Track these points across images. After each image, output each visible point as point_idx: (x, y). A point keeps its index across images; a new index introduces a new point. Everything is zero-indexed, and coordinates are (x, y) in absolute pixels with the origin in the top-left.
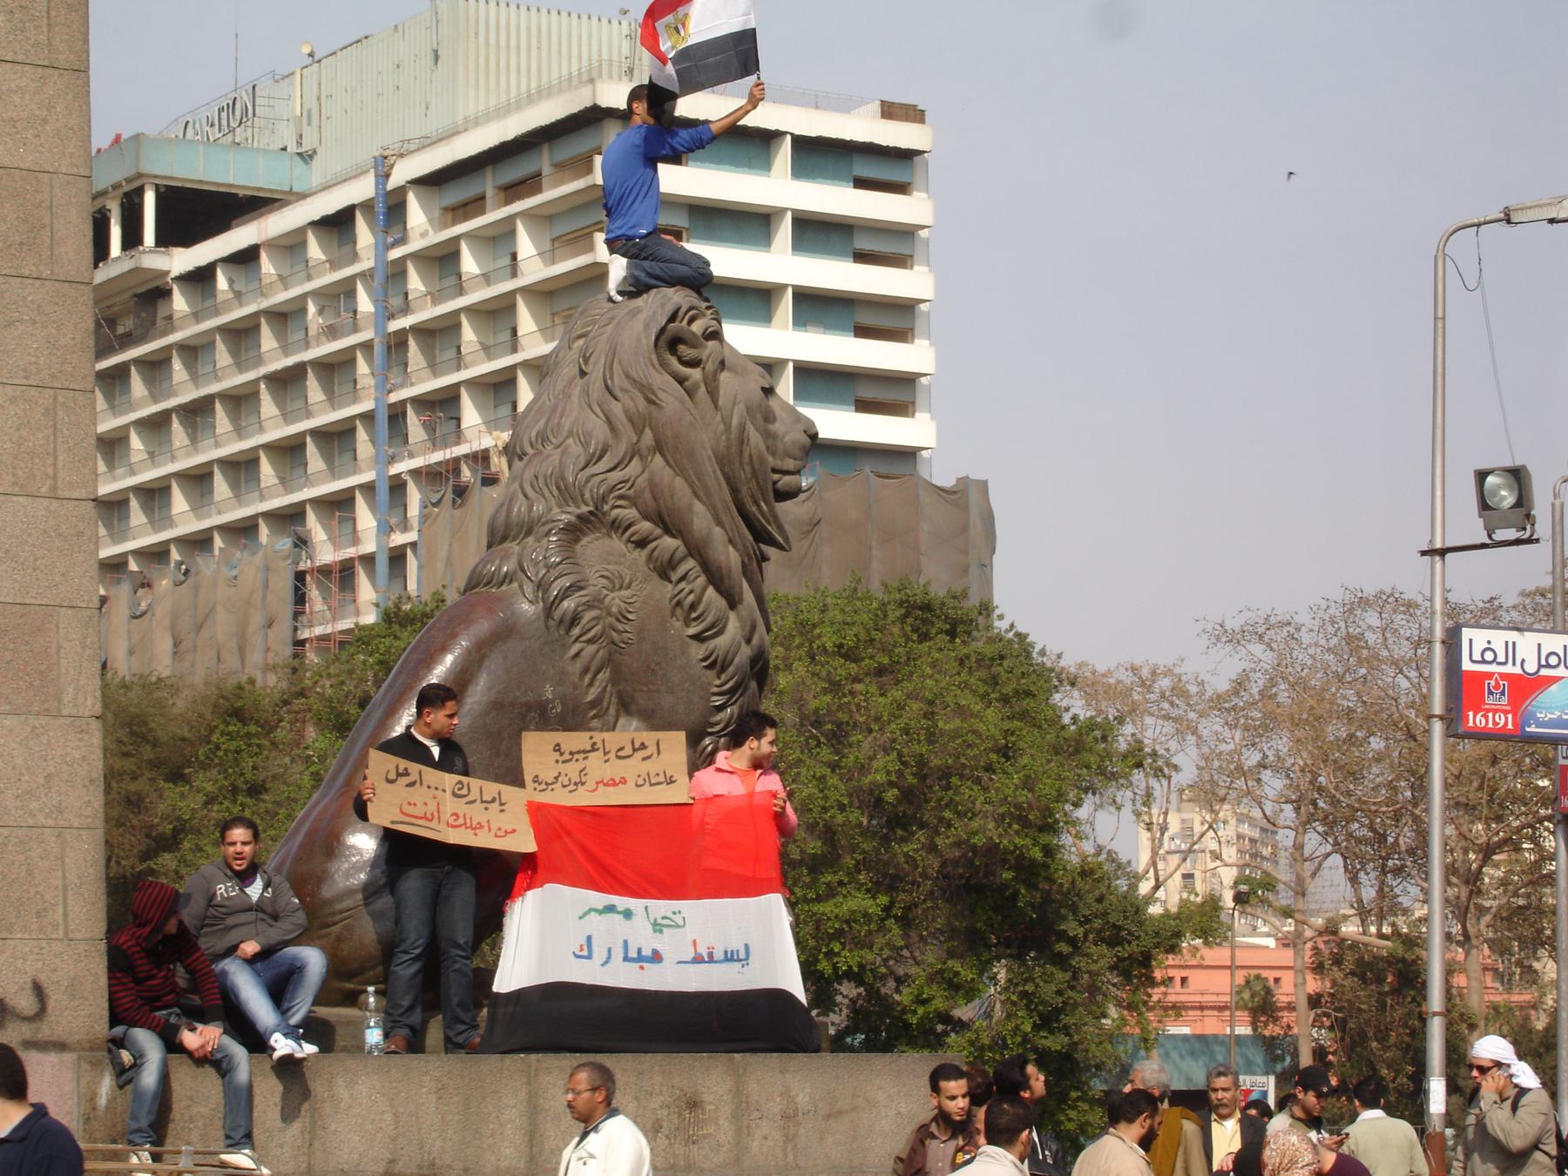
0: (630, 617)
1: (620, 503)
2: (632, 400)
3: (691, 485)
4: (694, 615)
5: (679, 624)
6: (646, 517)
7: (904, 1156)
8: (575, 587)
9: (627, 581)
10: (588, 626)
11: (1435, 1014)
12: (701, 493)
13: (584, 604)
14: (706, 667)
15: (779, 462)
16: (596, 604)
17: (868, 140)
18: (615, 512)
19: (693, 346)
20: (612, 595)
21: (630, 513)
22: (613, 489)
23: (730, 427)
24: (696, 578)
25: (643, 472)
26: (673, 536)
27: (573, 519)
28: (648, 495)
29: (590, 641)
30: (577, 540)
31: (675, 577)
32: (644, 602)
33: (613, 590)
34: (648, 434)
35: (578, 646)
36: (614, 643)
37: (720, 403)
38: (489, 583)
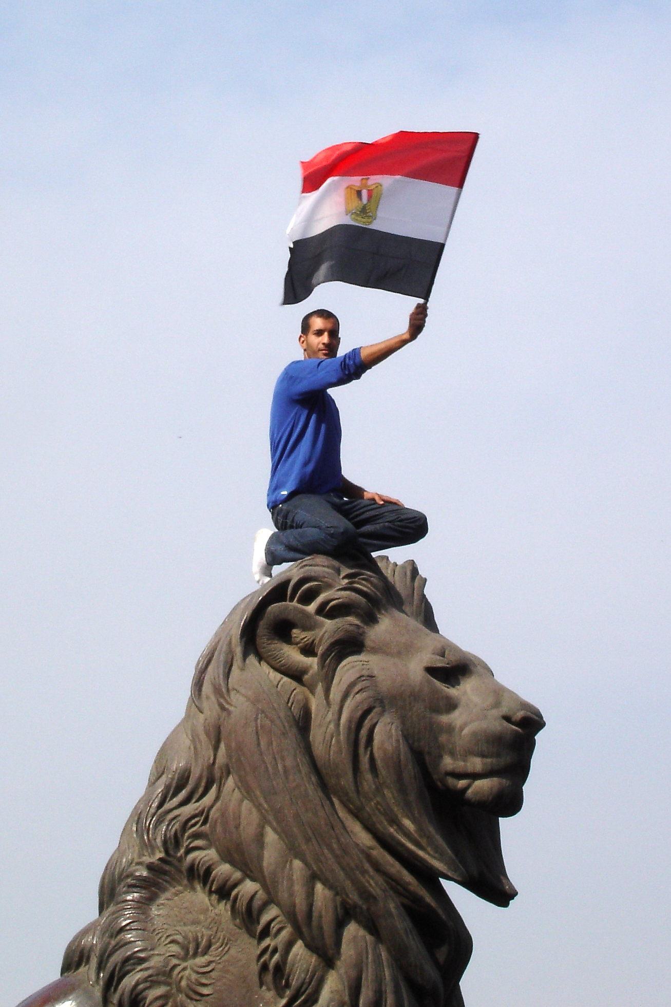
0: (205, 991)
1: (198, 843)
9: (204, 943)
13: (145, 980)
15: (461, 763)
18: (191, 857)
19: (305, 628)
20: (184, 965)
21: (209, 855)
22: (185, 826)
26: (253, 879)
32: (225, 971)
33: (185, 958)
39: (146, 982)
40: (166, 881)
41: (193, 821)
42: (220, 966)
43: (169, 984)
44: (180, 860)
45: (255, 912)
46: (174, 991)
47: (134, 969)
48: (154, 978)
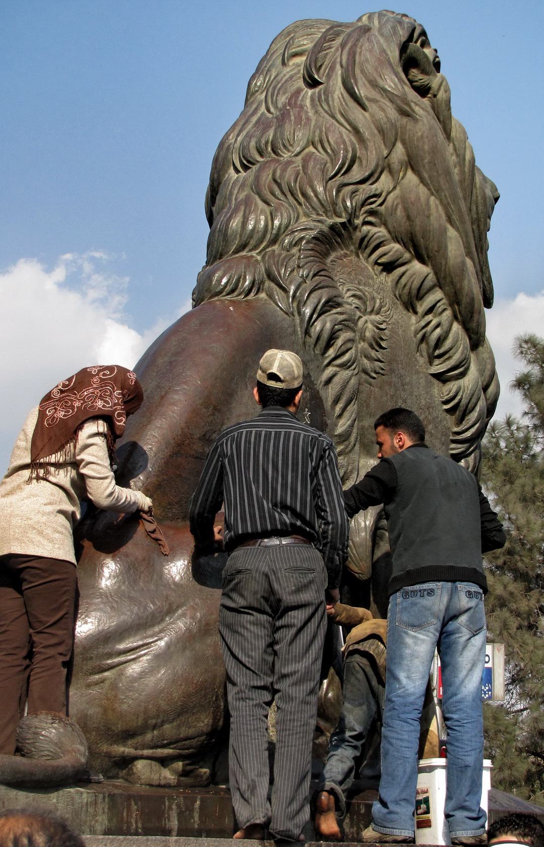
0: (383, 344)
1: (370, 219)
2: (383, 110)
3: (446, 207)
4: (437, 352)
5: (422, 360)
6: (396, 240)
7: (511, 813)
8: (331, 304)
10: (343, 348)
12: (455, 217)
13: (340, 323)
14: (447, 411)
18: (366, 228)
19: (424, 72)
21: (380, 232)
23: (464, 159)
24: (445, 310)
25: (395, 188)
26: (422, 261)
27: (325, 228)
28: (400, 212)
29: (343, 366)
30: (326, 255)
31: (422, 307)
33: (365, 313)
34: (399, 148)
35: (330, 371)
36: (365, 372)
37: (453, 134)
38: (233, 291)
39: (341, 324)
40: (337, 242)
41: (372, 200)
42: (390, 327)
43: (354, 331)
44: (356, 228)
45: (422, 291)
46: (357, 338)
47: (329, 311)
48: (346, 323)
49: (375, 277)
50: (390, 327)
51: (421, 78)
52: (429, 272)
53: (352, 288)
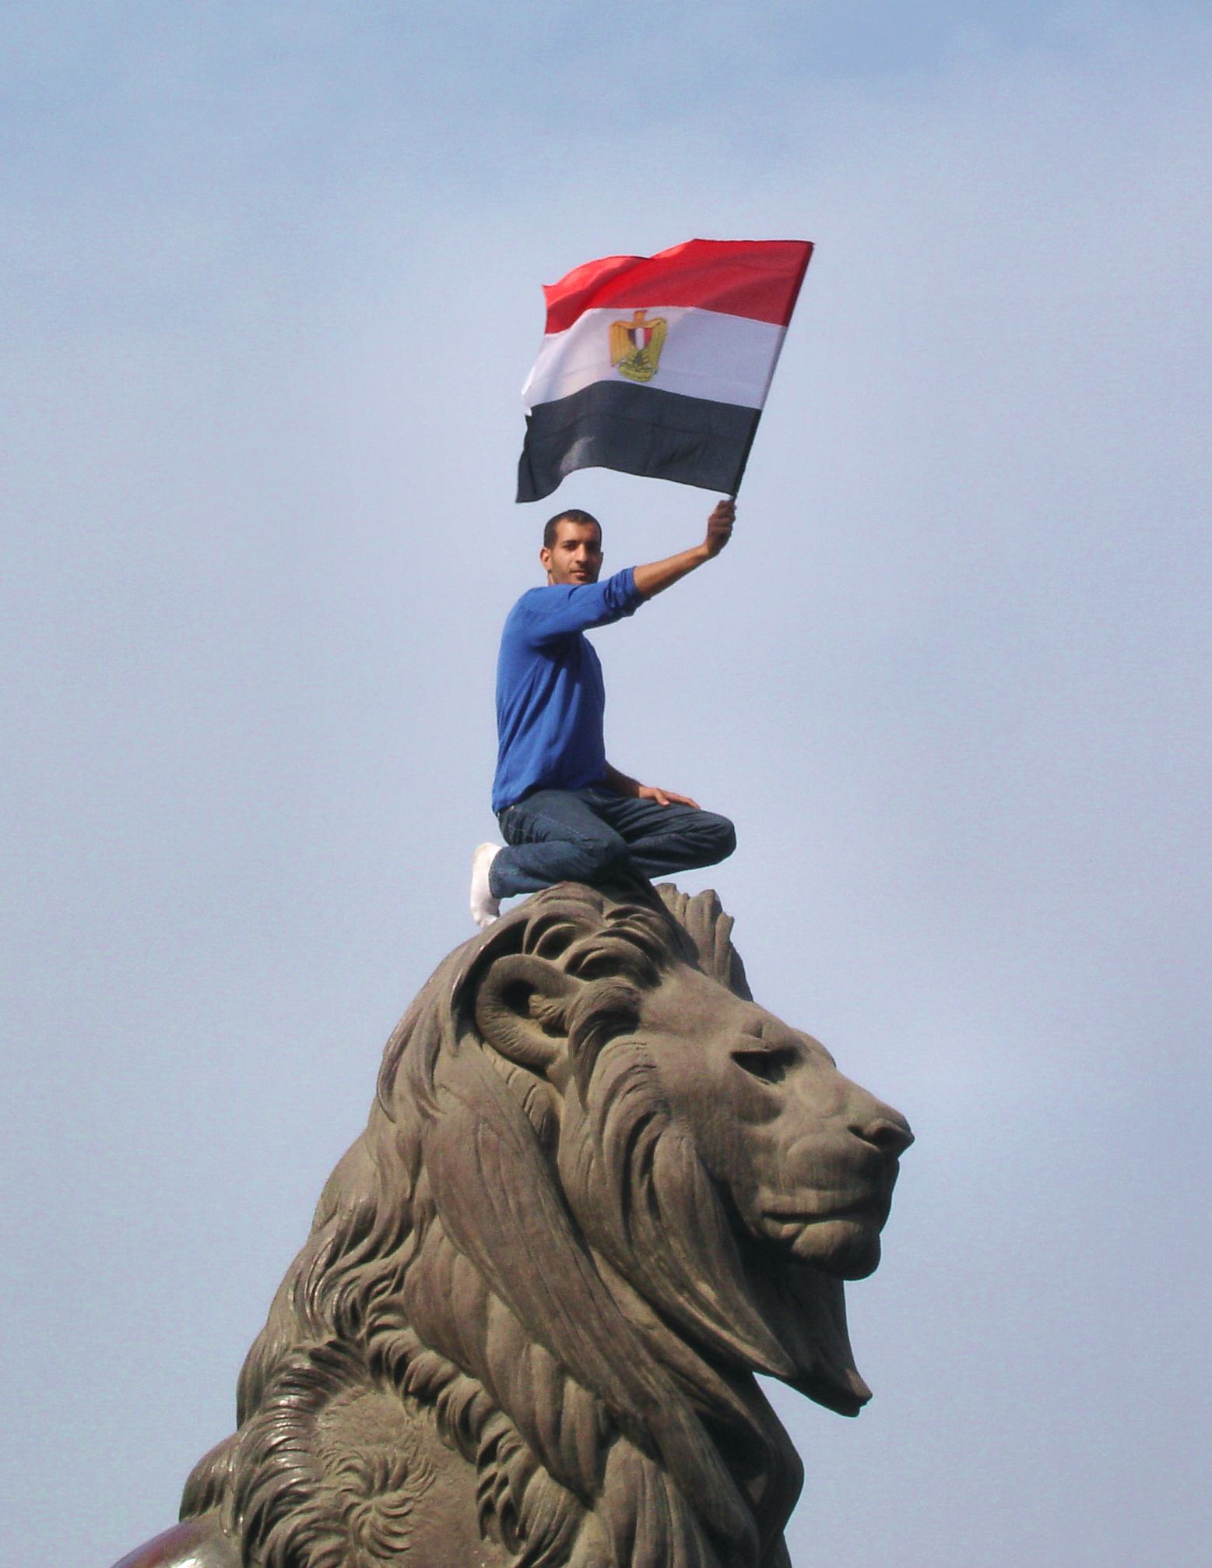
0: (398, 1543)
9: (396, 1471)
11: (475, 910)
13: (308, 1527)
16: (333, 1524)
17: (801, 1456)
18: (376, 1340)
20: (366, 1504)
22: (367, 1294)
24: (511, 1451)
26: (471, 1374)
33: (367, 1494)
41: (380, 1286)
42: (421, 1506)
43: (343, 1533)
44: (360, 1344)
46: (351, 1543)
47: (290, 1511)
49: (407, 1418)
50: (421, 1506)
51: (546, 1006)
52: (478, 1388)
53: (350, 1455)
